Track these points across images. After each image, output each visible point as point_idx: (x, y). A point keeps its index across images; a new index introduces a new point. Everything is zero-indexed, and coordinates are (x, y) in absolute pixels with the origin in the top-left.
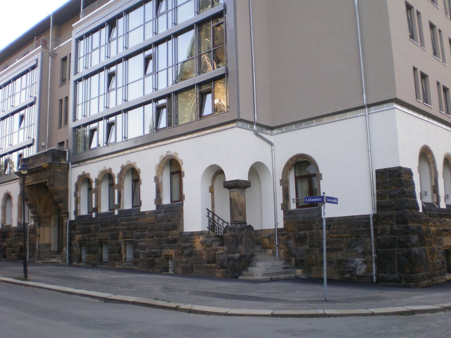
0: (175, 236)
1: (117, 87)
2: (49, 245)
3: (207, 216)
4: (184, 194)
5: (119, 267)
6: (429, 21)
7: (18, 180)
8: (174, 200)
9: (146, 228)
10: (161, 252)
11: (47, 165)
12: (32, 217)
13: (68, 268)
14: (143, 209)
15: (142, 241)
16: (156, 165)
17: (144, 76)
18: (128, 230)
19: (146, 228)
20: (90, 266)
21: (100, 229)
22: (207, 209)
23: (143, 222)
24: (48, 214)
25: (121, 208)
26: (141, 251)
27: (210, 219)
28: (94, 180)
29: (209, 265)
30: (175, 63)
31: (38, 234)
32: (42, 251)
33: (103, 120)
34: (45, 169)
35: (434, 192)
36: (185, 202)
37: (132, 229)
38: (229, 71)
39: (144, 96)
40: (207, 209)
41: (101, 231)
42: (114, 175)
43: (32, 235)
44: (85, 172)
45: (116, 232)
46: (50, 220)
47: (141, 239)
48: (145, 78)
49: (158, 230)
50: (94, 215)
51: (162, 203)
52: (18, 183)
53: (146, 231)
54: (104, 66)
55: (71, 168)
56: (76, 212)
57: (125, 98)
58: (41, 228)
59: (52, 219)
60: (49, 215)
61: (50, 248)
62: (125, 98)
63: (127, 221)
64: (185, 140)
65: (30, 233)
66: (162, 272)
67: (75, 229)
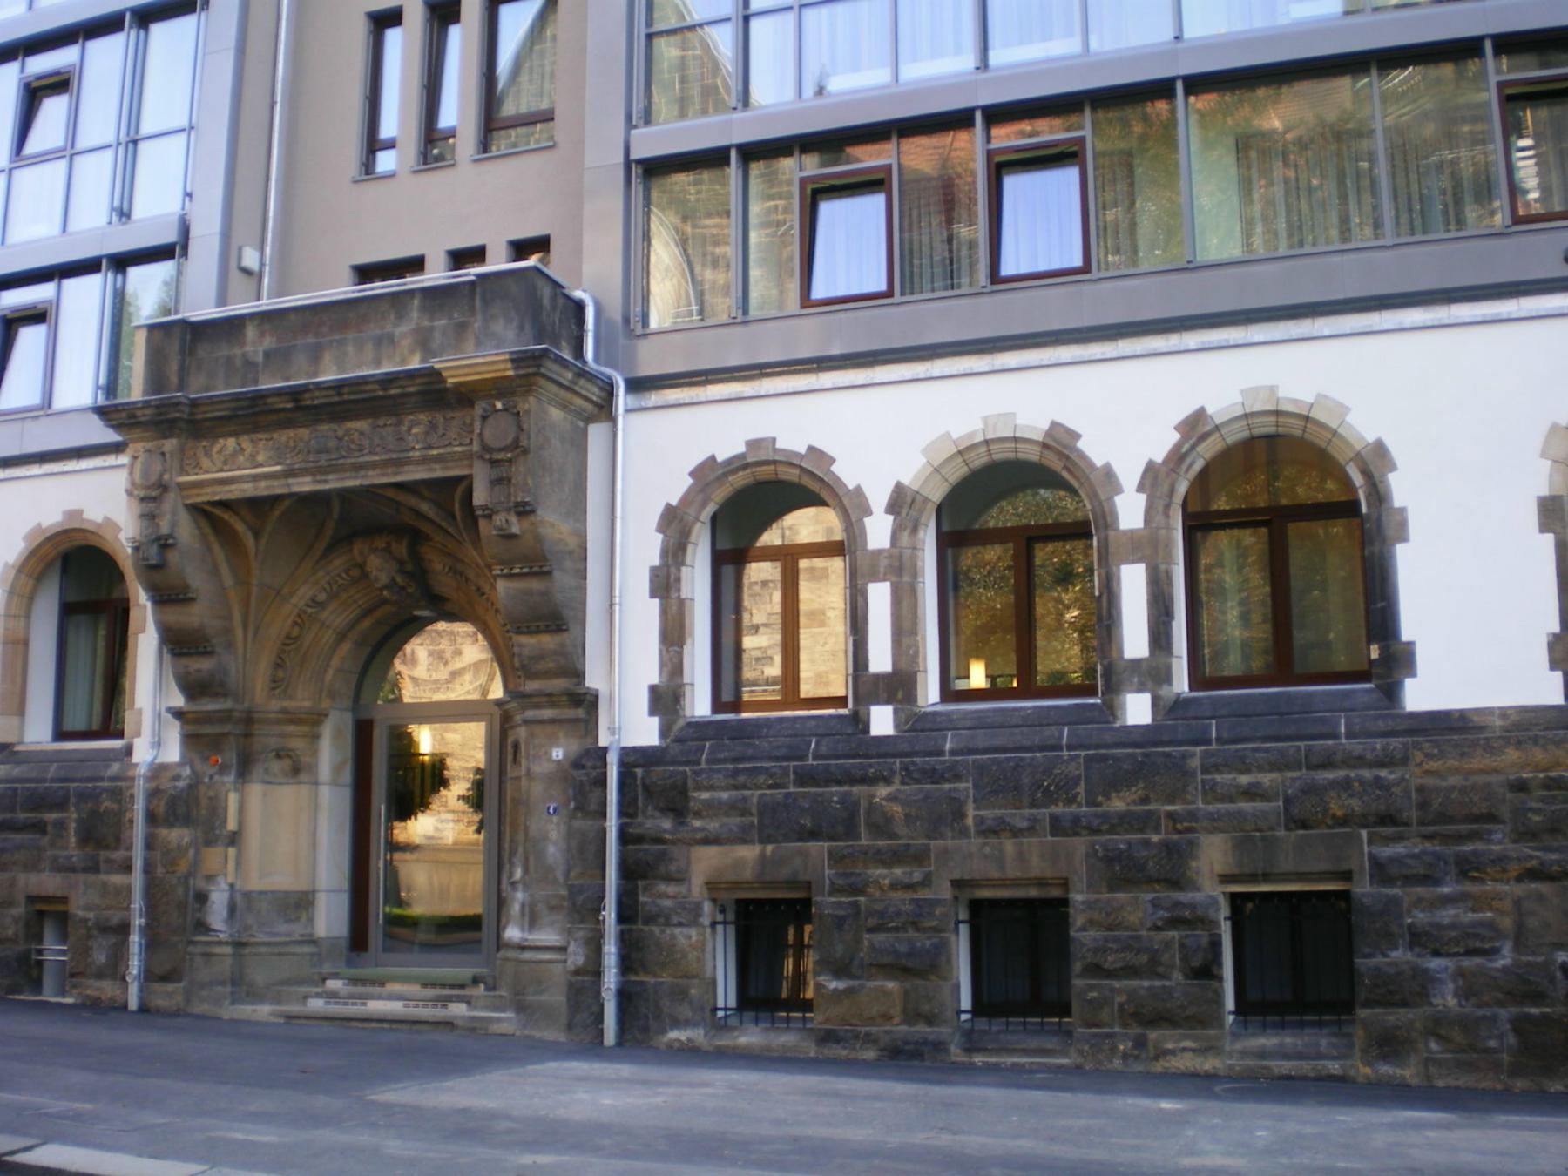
1: (73, 146)
2: (302, 903)
5: (1207, 1066)
7: (124, 459)
8: (70, 725)
11: (509, 365)
12: (178, 714)
13: (625, 1070)
15: (1447, 900)
17: (11, 161)
19: (1491, 818)
21: (971, 812)
23: (1453, 780)
24: (302, 701)
26: (1435, 964)
28: (878, 498)
30: (128, 134)
31: (232, 825)
32: (262, 938)
33: (173, 257)
34: (464, 396)
37: (1344, 821)
38: (192, 234)
39: (982, 76)
41: (989, 830)
42: (1108, 473)
43: (176, 836)
44: (86, 516)
45: (1155, 838)
46: (316, 737)
47: (1437, 882)
48: (16, 173)
50: (882, 721)
52: (120, 480)
53: (1490, 832)
54: (127, 9)
55: (628, 411)
56: (665, 699)
57: (122, 203)
58: (255, 790)
59: (327, 731)
60: (307, 704)
61: (311, 920)
62: (122, 203)
63: (1274, 767)
65: (151, 818)
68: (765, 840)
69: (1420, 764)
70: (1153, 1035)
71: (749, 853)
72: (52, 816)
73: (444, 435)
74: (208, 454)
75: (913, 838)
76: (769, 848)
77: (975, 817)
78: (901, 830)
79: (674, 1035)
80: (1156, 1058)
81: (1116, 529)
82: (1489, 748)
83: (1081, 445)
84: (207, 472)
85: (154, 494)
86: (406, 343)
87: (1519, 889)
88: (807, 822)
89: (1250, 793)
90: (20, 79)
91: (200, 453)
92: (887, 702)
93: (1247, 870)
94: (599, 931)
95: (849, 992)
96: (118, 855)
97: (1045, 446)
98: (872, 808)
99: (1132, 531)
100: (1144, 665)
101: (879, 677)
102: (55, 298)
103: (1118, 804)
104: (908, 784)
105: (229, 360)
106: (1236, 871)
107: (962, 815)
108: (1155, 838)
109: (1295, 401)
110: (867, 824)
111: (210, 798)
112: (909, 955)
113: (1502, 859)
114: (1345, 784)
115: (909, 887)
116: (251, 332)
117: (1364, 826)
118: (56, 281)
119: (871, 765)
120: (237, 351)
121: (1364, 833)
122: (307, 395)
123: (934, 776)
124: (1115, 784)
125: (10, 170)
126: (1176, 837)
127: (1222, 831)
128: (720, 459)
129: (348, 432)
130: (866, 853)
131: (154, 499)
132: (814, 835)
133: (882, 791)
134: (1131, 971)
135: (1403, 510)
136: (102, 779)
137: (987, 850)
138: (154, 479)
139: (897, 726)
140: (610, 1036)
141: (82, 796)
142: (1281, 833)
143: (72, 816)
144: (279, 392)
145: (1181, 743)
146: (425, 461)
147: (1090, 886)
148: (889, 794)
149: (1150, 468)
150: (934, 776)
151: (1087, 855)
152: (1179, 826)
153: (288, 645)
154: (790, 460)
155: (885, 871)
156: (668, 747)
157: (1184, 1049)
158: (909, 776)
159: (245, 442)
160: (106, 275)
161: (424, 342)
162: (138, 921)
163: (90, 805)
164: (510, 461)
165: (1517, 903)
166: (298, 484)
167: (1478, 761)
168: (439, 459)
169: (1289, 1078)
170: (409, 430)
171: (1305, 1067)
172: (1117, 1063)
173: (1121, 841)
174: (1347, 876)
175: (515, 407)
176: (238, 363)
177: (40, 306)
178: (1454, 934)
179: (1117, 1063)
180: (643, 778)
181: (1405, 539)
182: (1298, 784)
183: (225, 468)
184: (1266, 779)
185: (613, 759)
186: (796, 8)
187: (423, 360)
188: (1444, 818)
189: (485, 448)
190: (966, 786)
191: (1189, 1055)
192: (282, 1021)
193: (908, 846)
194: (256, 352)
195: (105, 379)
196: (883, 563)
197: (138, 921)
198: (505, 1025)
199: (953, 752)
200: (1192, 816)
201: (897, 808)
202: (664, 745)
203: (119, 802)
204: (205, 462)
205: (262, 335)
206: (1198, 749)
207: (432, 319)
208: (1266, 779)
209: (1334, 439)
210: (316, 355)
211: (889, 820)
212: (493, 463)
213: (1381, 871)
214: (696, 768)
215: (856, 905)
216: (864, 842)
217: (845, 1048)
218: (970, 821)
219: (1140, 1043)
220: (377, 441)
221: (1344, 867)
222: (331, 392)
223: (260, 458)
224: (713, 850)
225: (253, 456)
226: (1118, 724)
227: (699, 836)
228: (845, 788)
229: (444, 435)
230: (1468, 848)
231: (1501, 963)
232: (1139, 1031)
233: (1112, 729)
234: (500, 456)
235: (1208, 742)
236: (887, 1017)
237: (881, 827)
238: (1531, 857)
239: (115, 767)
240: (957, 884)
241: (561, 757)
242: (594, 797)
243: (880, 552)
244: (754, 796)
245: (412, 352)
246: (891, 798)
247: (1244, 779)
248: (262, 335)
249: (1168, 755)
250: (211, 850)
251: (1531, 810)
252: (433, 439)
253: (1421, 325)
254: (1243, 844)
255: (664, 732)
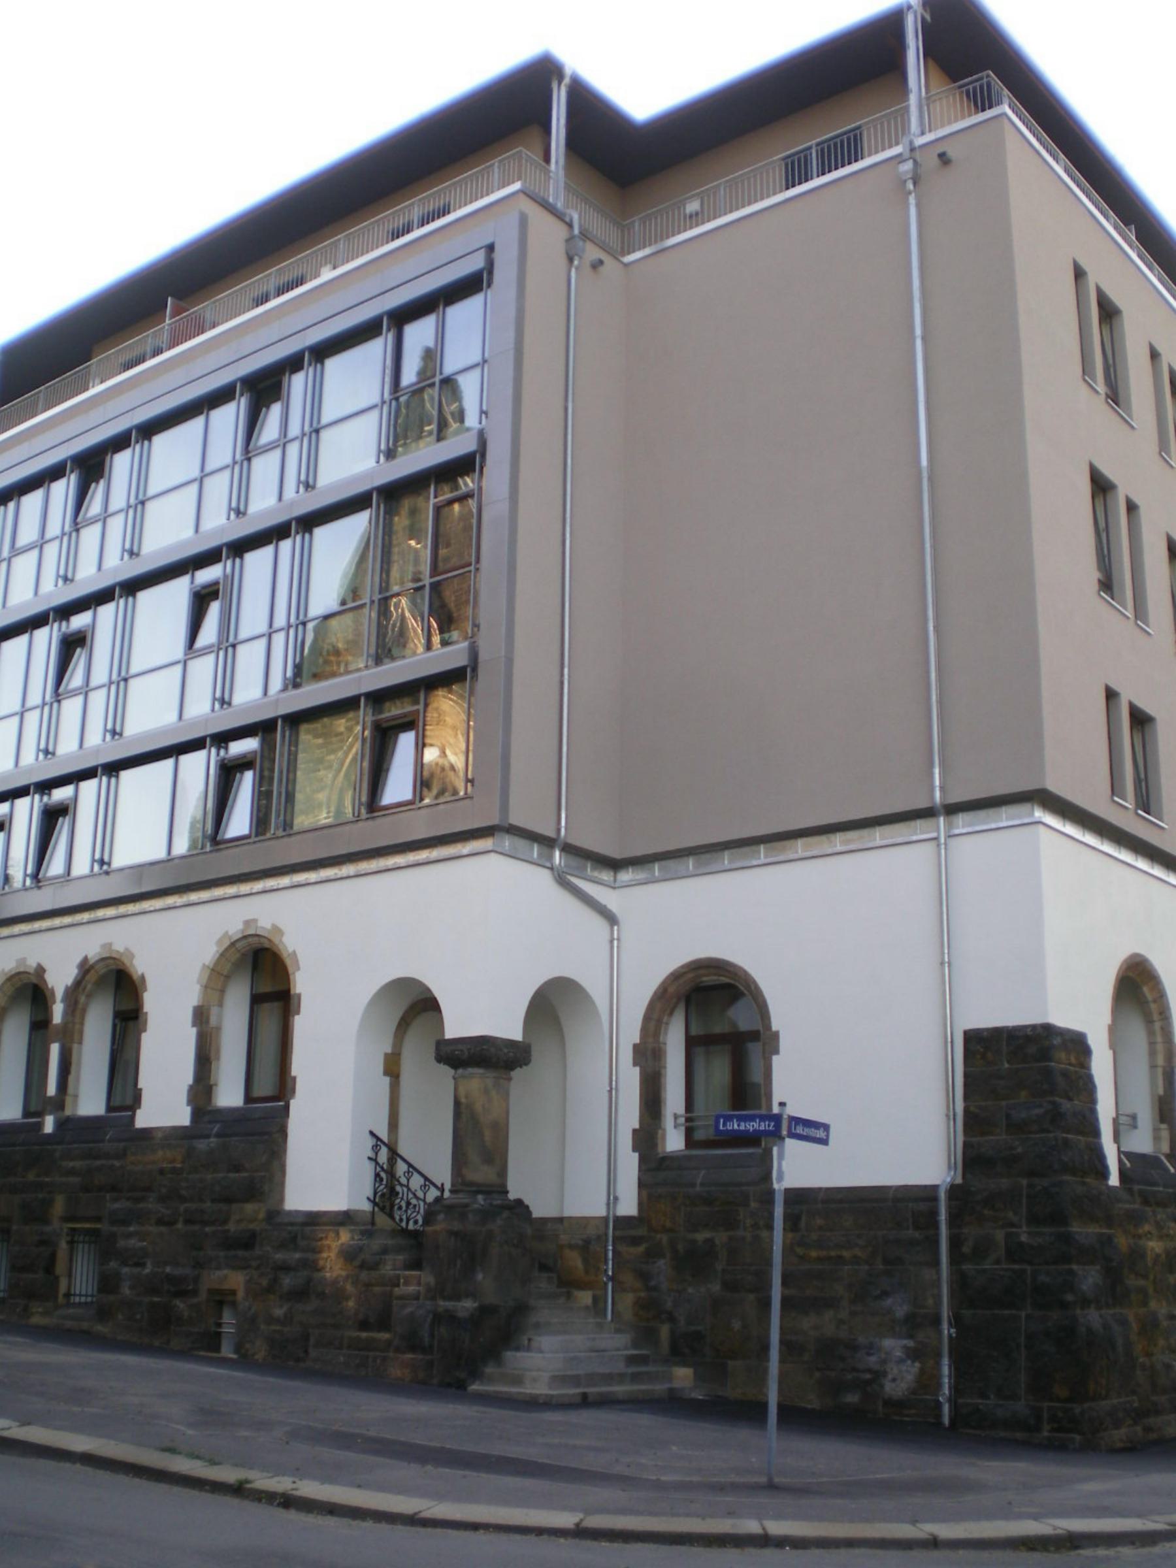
3: (370, 1158)
10: (196, 1280)
17: (186, 654)
22: (372, 1133)
25: (68, 1112)
27: (378, 1169)
40: (372, 1133)
51: (213, 1101)
54: (373, 489)
90: (191, 589)
101: (50, 1098)
102: (9, 814)
118: (10, 800)
125: (185, 662)
160: (101, 779)
169: (69, 1330)
177: (65, 802)
195: (33, 869)
206: (59, 1147)
231: (147, 1271)
253: (209, 899)
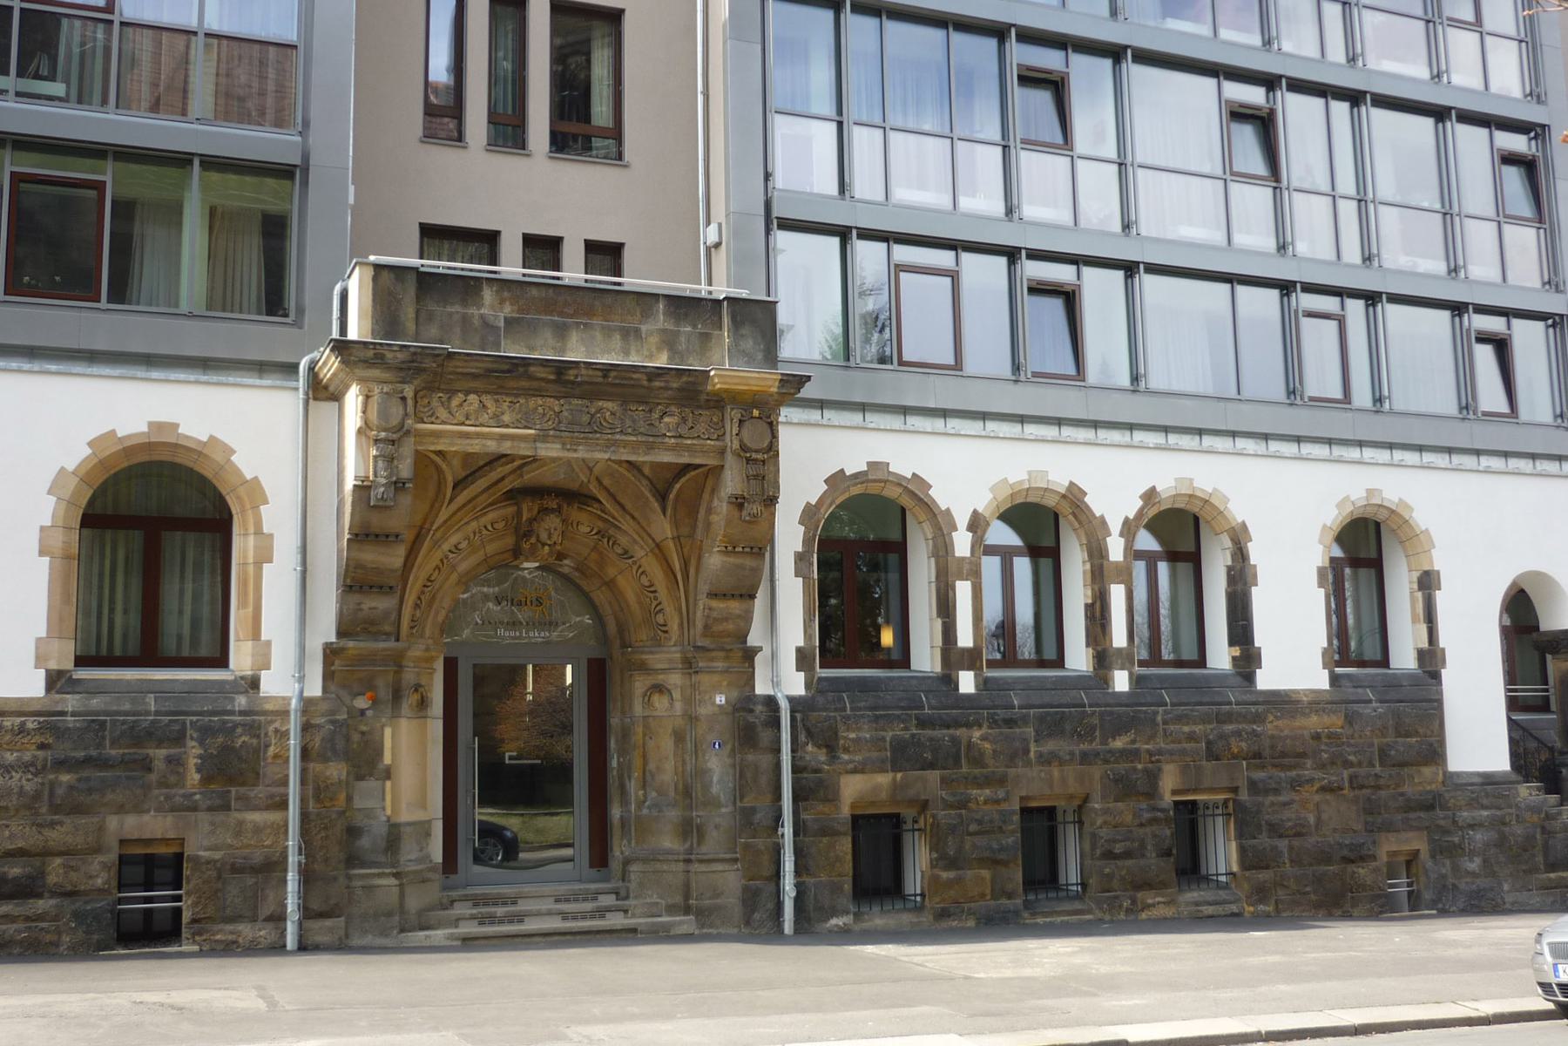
0: (1430, 784)
4: (1441, 646)
6: (784, 251)
9: (1303, 755)
14: (1266, 680)
16: (1325, 526)
18: (1212, 755)
19: (1303, 755)
20: (971, 923)
21: (1033, 748)
28: (962, 520)
29: (1552, 875)
35: (125, 840)
36: (1446, 675)
37: (1235, 757)
41: (1046, 760)
42: (1103, 521)
45: (1140, 766)
49: (1360, 764)
50: (967, 682)
64: (1048, 441)
66: (1385, 912)
67: (830, 745)
68: (895, 769)
69: (1272, 722)
70: (1139, 895)
71: (884, 779)
72: (159, 754)
73: (692, 427)
74: (446, 405)
75: (997, 767)
76: (899, 775)
77: (1036, 752)
78: (991, 762)
79: (834, 921)
80: (1142, 910)
81: (1108, 560)
82: (1304, 714)
83: (1087, 499)
84: (443, 423)
85: (395, 436)
86: (654, 340)
87: (1317, 798)
88: (928, 755)
89: (1191, 737)
91: (435, 403)
92: (969, 669)
93: (1187, 787)
94: (778, 844)
95: (958, 881)
96: (259, 792)
97: (1064, 496)
98: (970, 745)
99: (1117, 562)
100: (1124, 652)
101: (964, 650)
103: (1119, 743)
104: (992, 728)
105: (465, 320)
106: (1181, 787)
107: (1027, 751)
108: (1140, 766)
109: (1203, 490)
110: (967, 756)
111: (363, 733)
112: (1000, 850)
113: (1311, 781)
114: (1238, 734)
115: (997, 802)
116: (488, 295)
117: (1244, 759)
119: (970, 715)
120: (472, 311)
121: (1244, 763)
122: (572, 372)
123: (1010, 723)
124: (1117, 732)
126: (1150, 765)
127: (1173, 761)
128: (1131, 516)
129: (600, 410)
130: (966, 778)
131: (393, 442)
132: (932, 766)
133: (976, 734)
134: (1127, 854)
135: (1255, 566)
136: (232, 713)
137: (1043, 775)
138: (395, 422)
139: (977, 687)
140: (788, 927)
141: (206, 732)
142: (1204, 763)
143: (193, 753)
144: (545, 363)
145: (1151, 705)
146: (673, 449)
147: (1103, 797)
148: (981, 735)
149: (1126, 522)
150: (1010, 723)
151: (1101, 778)
152: (1153, 759)
153: (428, 587)
154: (899, 481)
155: (979, 791)
156: (813, 698)
157: (1159, 903)
158: (994, 723)
159: (488, 400)
161: (669, 342)
162: (293, 859)
163: (220, 740)
164: (764, 461)
165: (1317, 805)
166: (547, 448)
167: (1300, 722)
168: (689, 448)
170: (661, 418)
171: (1219, 910)
172: (1122, 916)
173: (1122, 767)
174: (1235, 790)
175: (769, 417)
176: (476, 322)
178: (1290, 824)
179: (1122, 916)
180: (803, 720)
181: (113, 432)
182: (1215, 732)
183: (467, 422)
184: (1198, 729)
185: (784, 705)
186: (883, 125)
187: (671, 360)
188: (1283, 755)
189: (744, 448)
190: (1030, 731)
191: (1161, 906)
192: (459, 943)
193: (993, 772)
194: (496, 317)
196: (966, 567)
197: (293, 859)
198: (685, 927)
199: (1021, 707)
200: (1160, 752)
201: (987, 745)
202: (810, 695)
203: (258, 736)
204: (442, 413)
205: (502, 302)
206: (1161, 709)
207: (677, 324)
208: (1198, 729)
209: (1218, 517)
210: (561, 332)
211: (982, 754)
212: (748, 460)
213: (1253, 786)
214: (843, 714)
215: (960, 816)
216: (964, 770)
217: (953, 920)
218: (1032, 755)
219: (1134, 902)
220: (628, 423)
221: (1235, 785)
222: (600, 373)
223: (506, 418)
224: (858, 777)
225: (496, 416)
226: (1110, 691)
227: (851, 766)
228: (951, 731)
229: (692, 427)
230: (1294, 773)
232: (1132, 893)
233: (1108, 693)
234: (754, 456)
235: (1166, 705)
236: (983, 896)
237: (977, 760)
238: (1324, 779)
239: (241, 701)
240: (1022, 798)
241: (723, 702)
242: (765, 736)
243: (963, 559)
244: (889, 735)
245: (659, 349)
246: (984, 738)
247: (1186, 729)
248: (502, 302)
249: (1145, 712)
250: (362, 784)
251: (1323, 750)
252: (683, 430)
254: (1184, 770)
255: (808, 686)
